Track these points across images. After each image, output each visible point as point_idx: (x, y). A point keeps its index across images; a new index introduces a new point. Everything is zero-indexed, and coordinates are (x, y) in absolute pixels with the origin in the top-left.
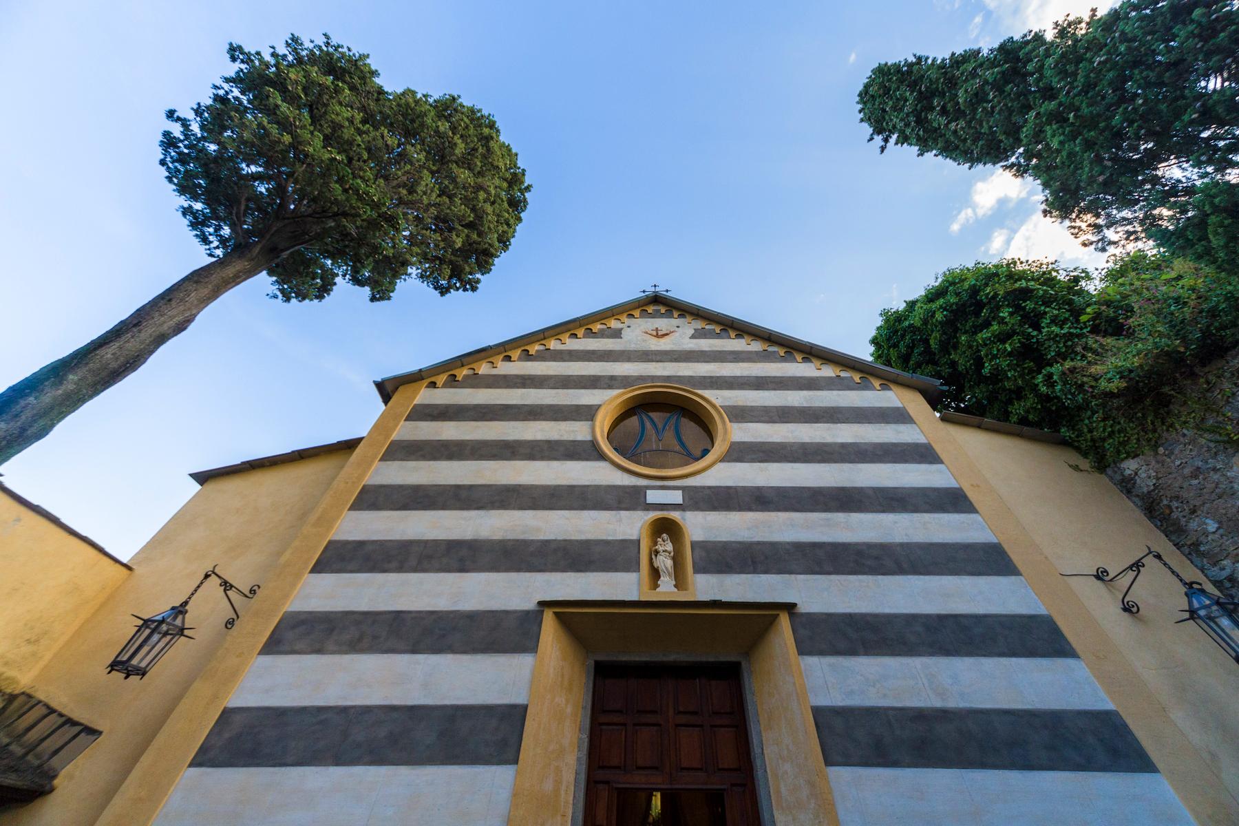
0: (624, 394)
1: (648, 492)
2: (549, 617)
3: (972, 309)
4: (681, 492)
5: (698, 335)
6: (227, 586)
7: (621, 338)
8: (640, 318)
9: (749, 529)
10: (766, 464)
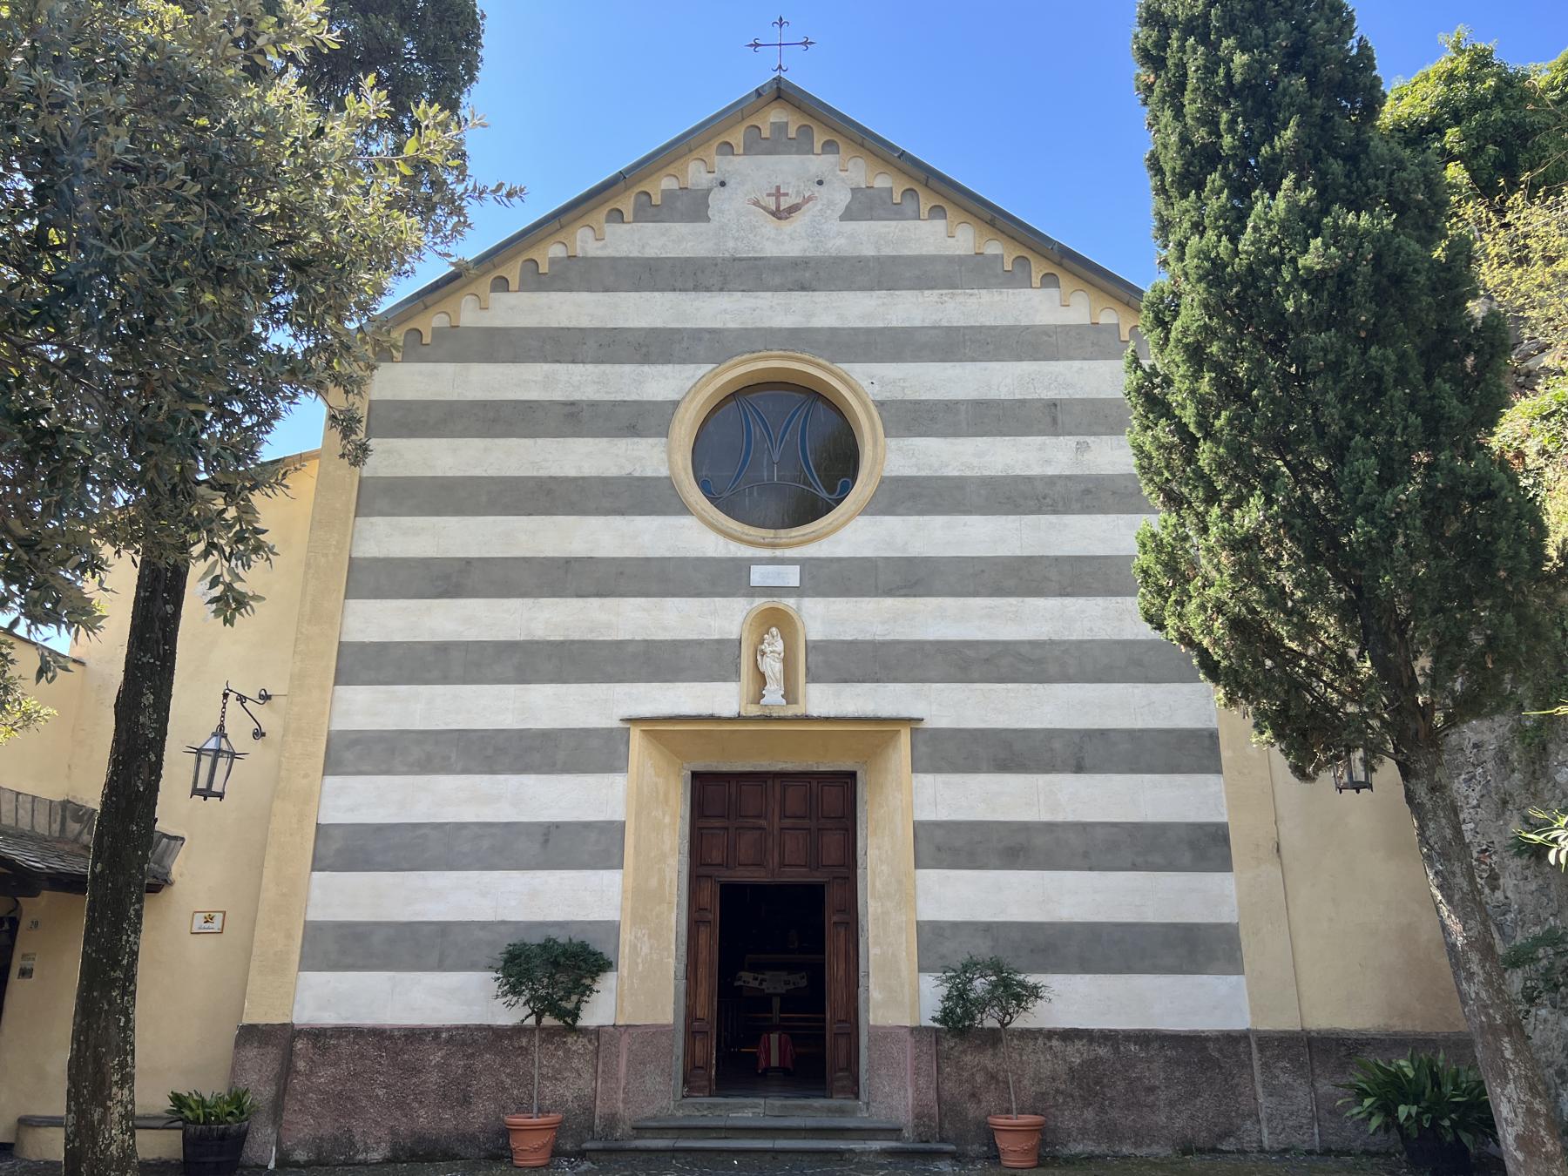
0: (715, 375)
2: (636, 733)
4: (798, 567)
5: (864, 206)
6: (242, 699)
7: (708, 220)
8: (744, 154)
10: (926, 518)
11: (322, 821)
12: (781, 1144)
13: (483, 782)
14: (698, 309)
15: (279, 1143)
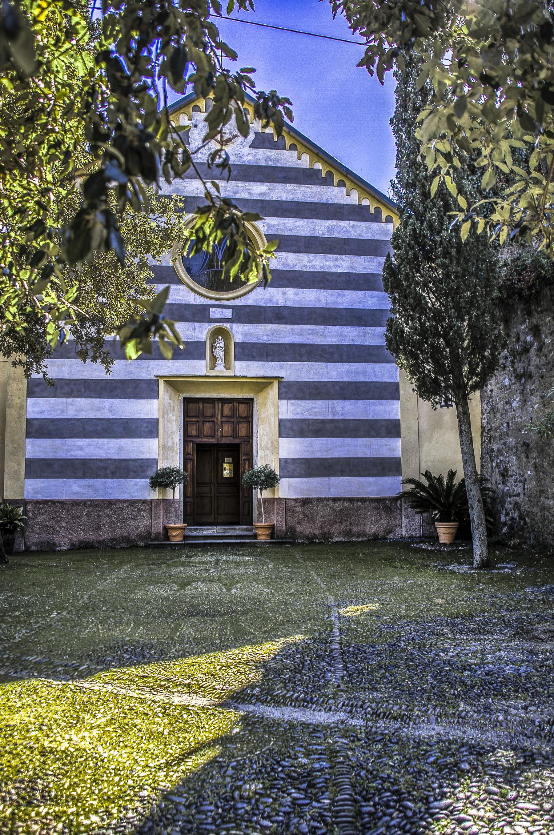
1: (211, 310)
3: (132, 625)
9: (268, 335)
11: (28, 417)
12: (225, 541)
13: (96, 401)
14: (185, 187)
15: (25, 544)
